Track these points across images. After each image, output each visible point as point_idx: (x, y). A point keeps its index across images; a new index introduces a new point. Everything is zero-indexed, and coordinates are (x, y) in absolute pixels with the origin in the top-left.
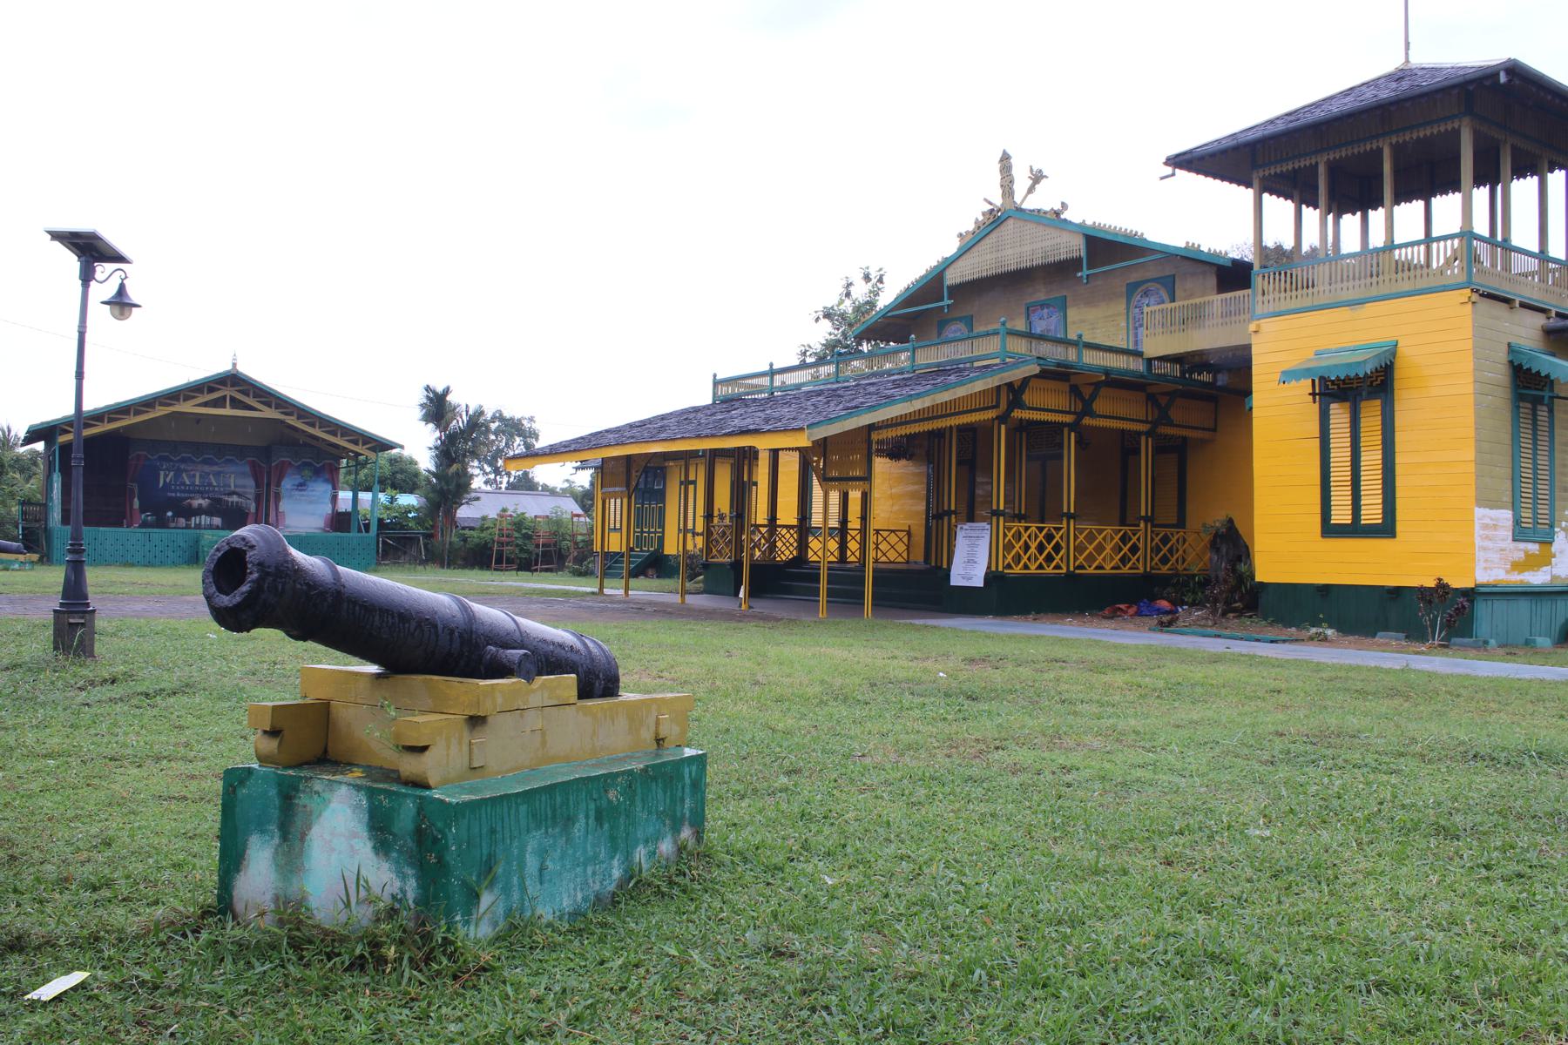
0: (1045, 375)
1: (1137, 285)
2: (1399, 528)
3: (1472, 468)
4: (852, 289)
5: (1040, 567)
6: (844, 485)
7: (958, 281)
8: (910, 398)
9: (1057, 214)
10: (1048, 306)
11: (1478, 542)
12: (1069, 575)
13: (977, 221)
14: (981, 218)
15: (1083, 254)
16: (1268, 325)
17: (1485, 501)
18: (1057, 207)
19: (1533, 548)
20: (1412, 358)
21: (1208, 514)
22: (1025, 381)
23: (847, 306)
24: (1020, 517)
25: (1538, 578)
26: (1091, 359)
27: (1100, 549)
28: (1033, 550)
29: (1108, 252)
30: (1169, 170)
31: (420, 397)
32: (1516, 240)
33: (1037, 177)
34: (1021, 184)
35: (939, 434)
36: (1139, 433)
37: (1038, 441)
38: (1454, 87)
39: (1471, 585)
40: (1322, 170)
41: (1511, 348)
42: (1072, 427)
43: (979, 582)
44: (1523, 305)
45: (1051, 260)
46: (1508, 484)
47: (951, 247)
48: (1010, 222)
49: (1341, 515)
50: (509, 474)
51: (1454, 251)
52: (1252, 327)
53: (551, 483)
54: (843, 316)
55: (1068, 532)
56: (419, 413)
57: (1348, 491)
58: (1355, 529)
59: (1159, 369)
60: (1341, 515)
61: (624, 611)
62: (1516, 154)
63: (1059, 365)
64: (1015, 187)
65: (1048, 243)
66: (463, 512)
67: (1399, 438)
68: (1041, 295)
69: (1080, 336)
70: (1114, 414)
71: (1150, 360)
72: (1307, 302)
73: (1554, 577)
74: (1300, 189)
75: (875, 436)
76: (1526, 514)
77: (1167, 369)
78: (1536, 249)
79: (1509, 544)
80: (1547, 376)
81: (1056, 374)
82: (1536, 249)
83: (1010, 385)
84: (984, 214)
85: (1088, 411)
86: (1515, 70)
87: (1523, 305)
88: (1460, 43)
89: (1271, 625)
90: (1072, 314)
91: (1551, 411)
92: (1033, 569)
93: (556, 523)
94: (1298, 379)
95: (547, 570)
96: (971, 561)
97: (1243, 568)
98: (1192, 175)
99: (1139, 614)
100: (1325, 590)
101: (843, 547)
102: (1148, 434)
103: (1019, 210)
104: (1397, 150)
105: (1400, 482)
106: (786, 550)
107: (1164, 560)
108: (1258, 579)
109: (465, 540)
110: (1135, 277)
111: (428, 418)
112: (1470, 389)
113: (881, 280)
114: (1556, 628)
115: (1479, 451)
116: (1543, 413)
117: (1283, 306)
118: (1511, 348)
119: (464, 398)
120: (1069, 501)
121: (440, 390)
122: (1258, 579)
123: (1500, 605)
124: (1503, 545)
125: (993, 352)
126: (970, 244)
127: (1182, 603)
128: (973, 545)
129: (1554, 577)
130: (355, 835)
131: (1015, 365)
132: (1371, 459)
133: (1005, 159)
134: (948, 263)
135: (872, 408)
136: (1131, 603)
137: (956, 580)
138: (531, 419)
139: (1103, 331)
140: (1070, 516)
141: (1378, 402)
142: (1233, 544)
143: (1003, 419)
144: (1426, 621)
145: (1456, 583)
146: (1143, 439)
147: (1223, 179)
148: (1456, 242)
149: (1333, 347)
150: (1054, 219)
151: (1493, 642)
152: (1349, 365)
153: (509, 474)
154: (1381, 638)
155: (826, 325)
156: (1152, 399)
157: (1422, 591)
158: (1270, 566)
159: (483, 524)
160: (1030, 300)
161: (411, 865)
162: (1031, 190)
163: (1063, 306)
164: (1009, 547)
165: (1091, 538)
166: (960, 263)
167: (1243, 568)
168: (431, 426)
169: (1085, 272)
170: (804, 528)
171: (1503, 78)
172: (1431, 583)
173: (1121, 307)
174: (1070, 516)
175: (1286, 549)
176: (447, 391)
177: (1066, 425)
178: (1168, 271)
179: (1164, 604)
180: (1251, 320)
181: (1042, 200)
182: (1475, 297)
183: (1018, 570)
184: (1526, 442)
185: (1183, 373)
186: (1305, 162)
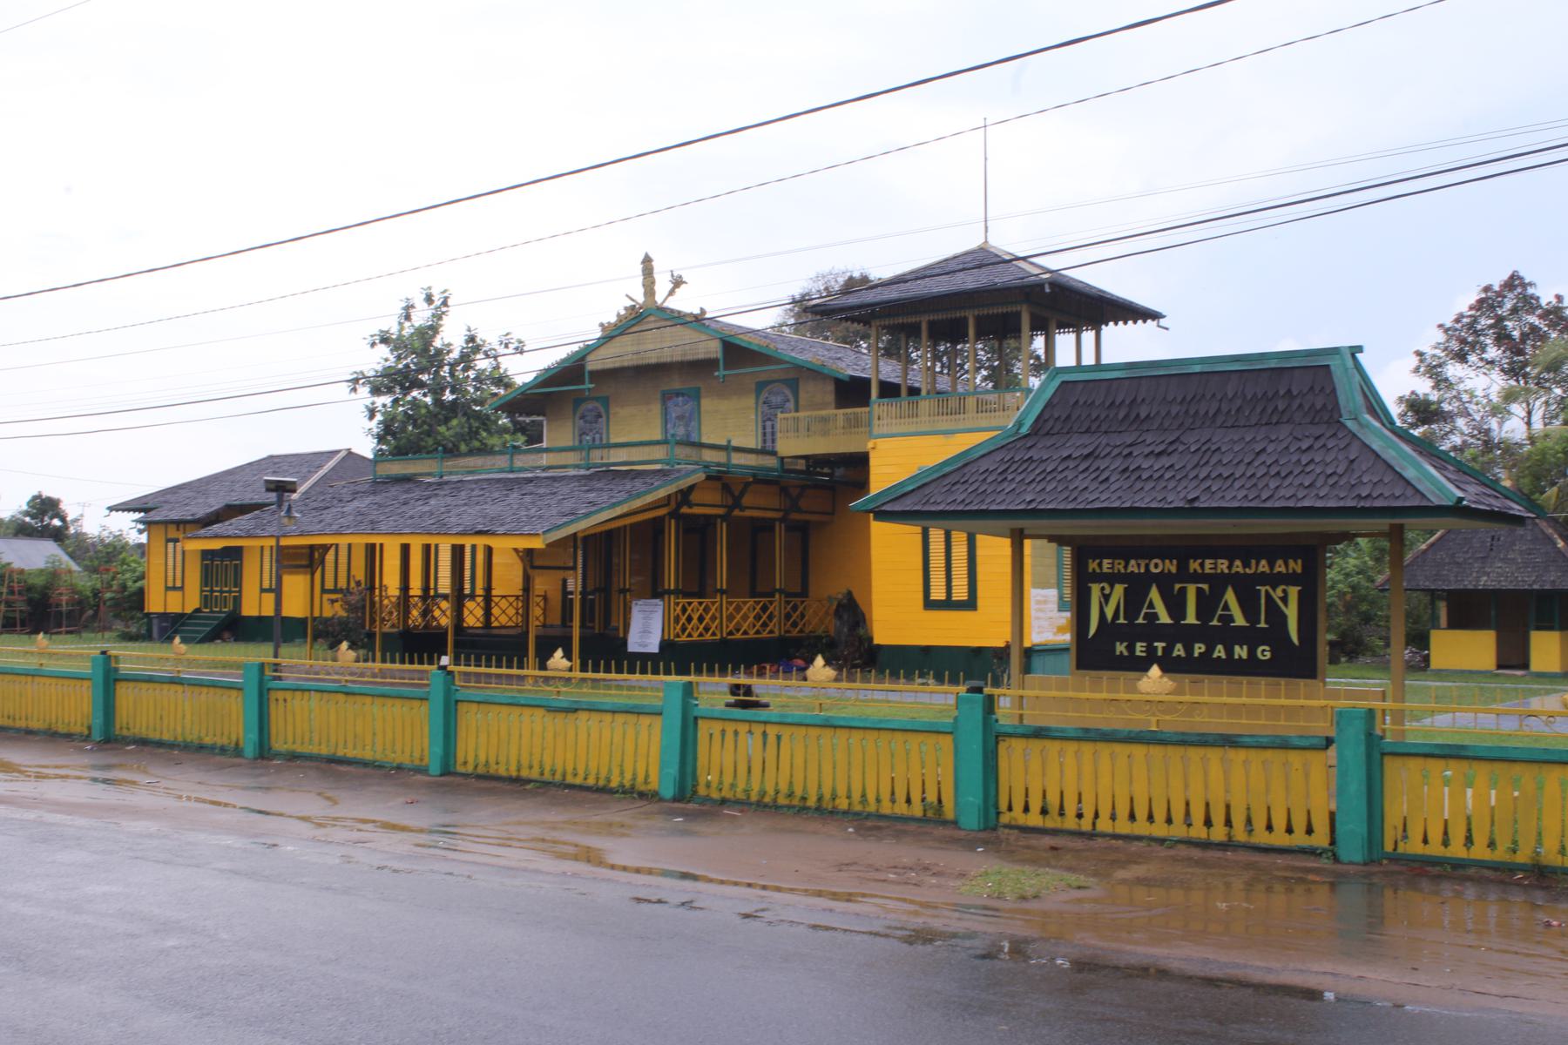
2: (980, 603)
5: (701, 635)
8: (613, 506)
12: (723, 641)
14: (623, 312)
15: (720, 355)
21: (827, 588)
22: (691, 488)
24: (686, 595)
26: (738, 459)
27: (745, 618)
28: (695, 621)
31: (642, 257)
33: (678, 282)
34: (662, 287)
37: (698, 532)
40: (924, 327)
42: (723, 518)
43: (654, 648)
49: (938, 594)
55: (717, 604)
57: (942, 575)
58: (948, 604)
60: (938, 594)
64: (656, 288)
68: (676, 384)
70: (758, 505)
72: (913, 429)
79: (1055, 614)
81: (719, 478)
90: (706, 404)
93: (54, 575)
95: (68, 632)
96: (646, 631)
97: (861, 631)
100: (927, 650)
102: (782, 520)
105: (980, 569)
107: (795, 624)
108: (876, 641)
110: (763, 378)
113: (445, 303)
117: (895, 430)
120: (722, 577)
122: (876, 641)
126: (611, 334)
132: (170, 573)
133: (647, 262)
135: (587, 515)
136: (773, 663)
139: (731, 427)
140: (722, 592)
142: (853, 612)
150: (698, 321)
155: (384, 351)
156: (784, 490)
158: (883, 633)
160: (666, 388)
162: (671, 293)
163: (696, 396)
164: (677, 619)
165: (738, 609)
167: (861, 631)
169: (720, 373)
170: (459, 598)
173: (657, 408)
174: (722, 592)
175: (896, 618)
181: (684, 302)
183: (684, 638)
186: (912, 319)
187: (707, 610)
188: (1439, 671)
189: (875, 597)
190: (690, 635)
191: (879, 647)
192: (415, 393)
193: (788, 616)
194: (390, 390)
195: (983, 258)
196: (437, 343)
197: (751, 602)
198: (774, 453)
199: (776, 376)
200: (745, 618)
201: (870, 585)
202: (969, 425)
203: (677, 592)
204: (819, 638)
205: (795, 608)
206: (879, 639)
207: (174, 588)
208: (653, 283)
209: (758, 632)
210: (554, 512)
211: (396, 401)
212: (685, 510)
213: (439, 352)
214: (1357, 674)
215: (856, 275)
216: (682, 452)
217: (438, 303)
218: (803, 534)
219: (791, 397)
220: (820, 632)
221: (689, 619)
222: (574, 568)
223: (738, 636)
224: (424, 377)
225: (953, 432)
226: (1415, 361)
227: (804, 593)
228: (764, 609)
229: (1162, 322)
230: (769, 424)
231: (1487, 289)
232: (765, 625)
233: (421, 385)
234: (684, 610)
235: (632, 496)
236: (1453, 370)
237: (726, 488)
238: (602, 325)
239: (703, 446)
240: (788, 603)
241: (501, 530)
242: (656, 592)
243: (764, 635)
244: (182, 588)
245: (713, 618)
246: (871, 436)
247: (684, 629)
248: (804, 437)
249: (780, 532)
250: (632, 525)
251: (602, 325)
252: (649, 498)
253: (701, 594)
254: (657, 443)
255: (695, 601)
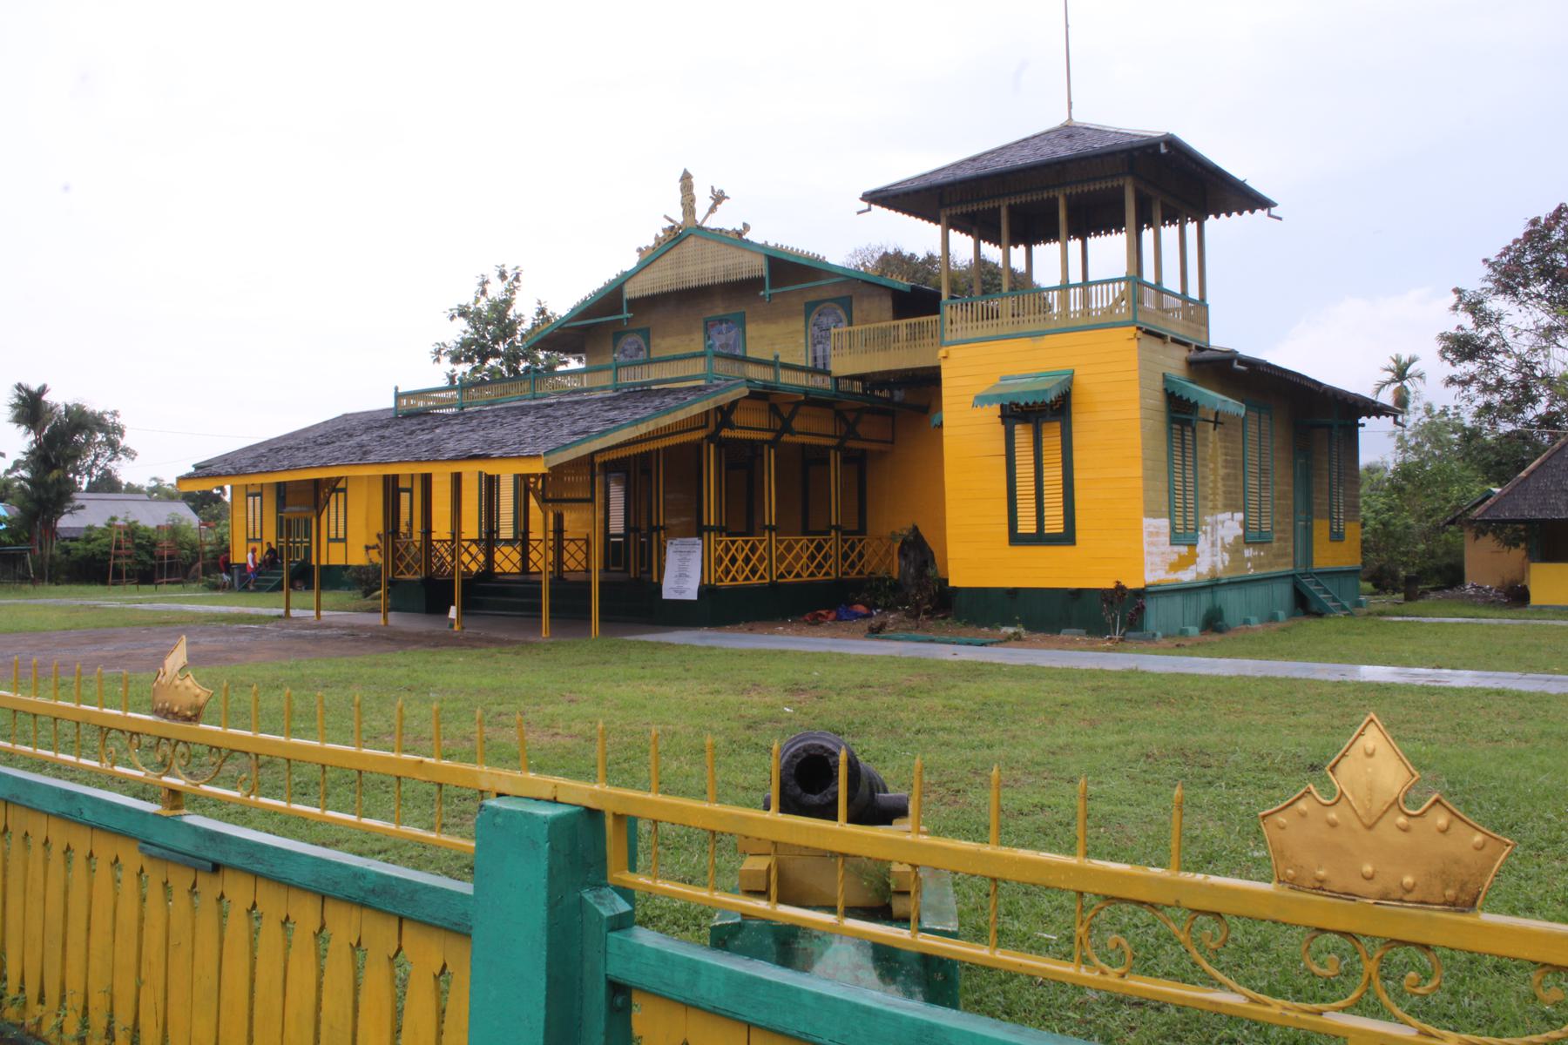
0: (754, 395)
1: (816, 304)
2: (1078, 536)
3: (1140, 483)
4: (488, 287)
5: (747, 578)
6: (558, 507)
7: (638, 295)
8: (636, 422)
9: (740, 234)
10: (727, 321)
11: (1146, 548)
13: (657, 237)
14: (661, 234)
15: (765, 273)
16: (957, 352)
17: (1152, 513)
18: (739, 227)
19: (1184, 550)
20: (1088, 385)
21: (890, 522)
22: (734, 405)
23: (483, 304)
25: (1187, 576)
26: (787, 378)
27: (798, 558)
28: (740, 557)
29: (789, 273)
30: (865, 205)
32: (1166, 285)
33: (719, 198)
34: (702, 203)
35: (646, 456)
36: (828, 448)
37: (741, 462)
38: (1122, 151)
39: (1142, 586)
40: (1004, 212)
41: (1166, 379)
43: (691, 594)
44: (1174, 341)
45: (733, 278)
46: (1166, 498)
47: (631, 262)
48: (692, 239)
49: (1027, 525)
50: (90, 474)
51: (1121, 293)
52: (942, 353)
53: (136, 482)
54: (478, 313)
55: (767, 543)
56: (7, 413)
58: (1040, 538)
59: (844, 386)
60: (1027, 525)
61: (317, 639)
62: (1164, 207)
63: (765, 387)
64: (696, 206)
65: (730, 262)
66: (65, 522)
67: (1077, 456)
68: (719, 310)
69: (777, 357)
70: (811, 430)
71: (837, 379)
72: (993, 332)
73: (1199, 574)
74: (983, 229)
75: (598, 460)
76: (1179, 521)
77: (858, 387)
78: (1178, 291)
79: (1167, 548)
80: (1196, 404)
81: (762, 395)
82: (1178, 291)
83: (719, 409)
84: (664, 230)
85: (787, 428)
86: (1172, 143)
87: (1174, 341)
88: (1127, 110)
89: (965, 624)
90: (752, 329)
91: (1194, 431)
92: (740, 581)
93: (174, 530)
94: (990, 404)
96: (682, 575)
98: (885, 210)
99: (839, 618)
100: (1013, 593)
101: (525, 557)
102: (837, 448)
103: (700, 228)
104: (1068, 198)
105: (1079, 496)
106: (472, 561)
107: (852, 566)
108: (951, 584)
109: (67, 551)
110: (812, 297)
111: (19, 420)
112: (1137, 414)
113: (517, 279)
114: (1200, 620)
115: (1145, 469)
116: (1188, 434)
117: (970, 335)
118: (1166, 379)
119: (59, 398)
120: (770, 513)
121: (34, 387)
122: (951, 584)
123: (1163, 602)
124: (1163, 549)
125: (684, 366)
126: (650, 259)
127: (876, 607)
128: (684, 560)
129: (1199, 574)
130: (858, 967)
131: (728, 388)
132: (1053, 474)
133: (686, 179)
134: (626, 277)
135: (602, 433)
136: (830, 608)
137: (668, 594)
138: (115, 414)
139: (779, 345)
140: (771, 529)
141: (1058, 424)
142: (920, 551)
143: (710, 438)
144: (1109, 619)
145: (1132, 584)
146: (832, 453)
147: (910, 214)
148: (1123, 285)
149: (1016, 374)
150: (736, 239)
151: (1159, 634)
152: (1037, 392)
153: (90, 474)
154: (1065, 635)
155: (462, 324)
156: (840, 415)
157: (1103, 593)
159: (89, 535)
160: (709, 315)
161: (919, 985)
162: (712, 210)
163: (740, 322)
164: (720, 560)
165: (789, 548)
166: (640, 277)
168: (23, 428)
169: (767, 291)
170: (489, 540)
171: (1163, 150)
172: (1112, 585)
173: (799, 324)
174: (771, 529)
175: (975, 555)
176: (43, 390)
177: (764, 442)
178: (844, 293)
179: (861, 609)
180: (941, 345)
181: (725, 219)
182: (1139, 334)
183: (727, 582)
184: (1178, 459)
185: (865, 389)
186: (988, 205)
187: (753, 549)
188: (1541, 608)
189: (950, 531)
190: (734, 579)
191: (955, 588)
192: (492, 362)
193: (845, 557)
194: (469, 359)
195: (1069, 131)
196: (511, 314)
197: (804, 540)
198: (826, 373)
199: (825, 295)
200: (798, 558)
201: (944, 519)
202: (1006, 331)
203: (720, 530)
204: (882, 580)
205: (852, 548)
206: (954, 582)
207: (337, 540)
208: (693, 200)
209: (812, 574)
210: (565, 431)
211: (475, 370)
212: (726, 433)
213: (513, 323)
214: (1472, 612)
215: (891, 251)
216: (722, 367)
217: (510, 279)
218: (858, 463)
219: (843, 317)
220: (881, 573)
221: (733, 560)
222: (591, 500)
223: (790, 579)
224: (501, 347)
225: (1042, 334)
226: (1454, 298)
227: (862, 530)
228: (819, 548)
229: (1274, 211)
230: (819, 347)
231: (1534, 222)
232: (820, 566)
233: (496, 354)
234: (727, 550)
235: (659, 412)
236: (1497, 304)
237: (774, 409)
238: (640, 250)
239: (745, 360)
240: (845, 541)
241: (497, 453)
242: (699, 530)
243: (820, 577)
244: (344, 540)
245: (761, 559)
246: (942, 344)
247: (727, 572)
248: (860, 352)
249: (835, 459)
250: (665, 448)
251: (640, 250)
252: (681, 415)
253: (749, 532)
254: (694, 356)
255: (740, 540)
